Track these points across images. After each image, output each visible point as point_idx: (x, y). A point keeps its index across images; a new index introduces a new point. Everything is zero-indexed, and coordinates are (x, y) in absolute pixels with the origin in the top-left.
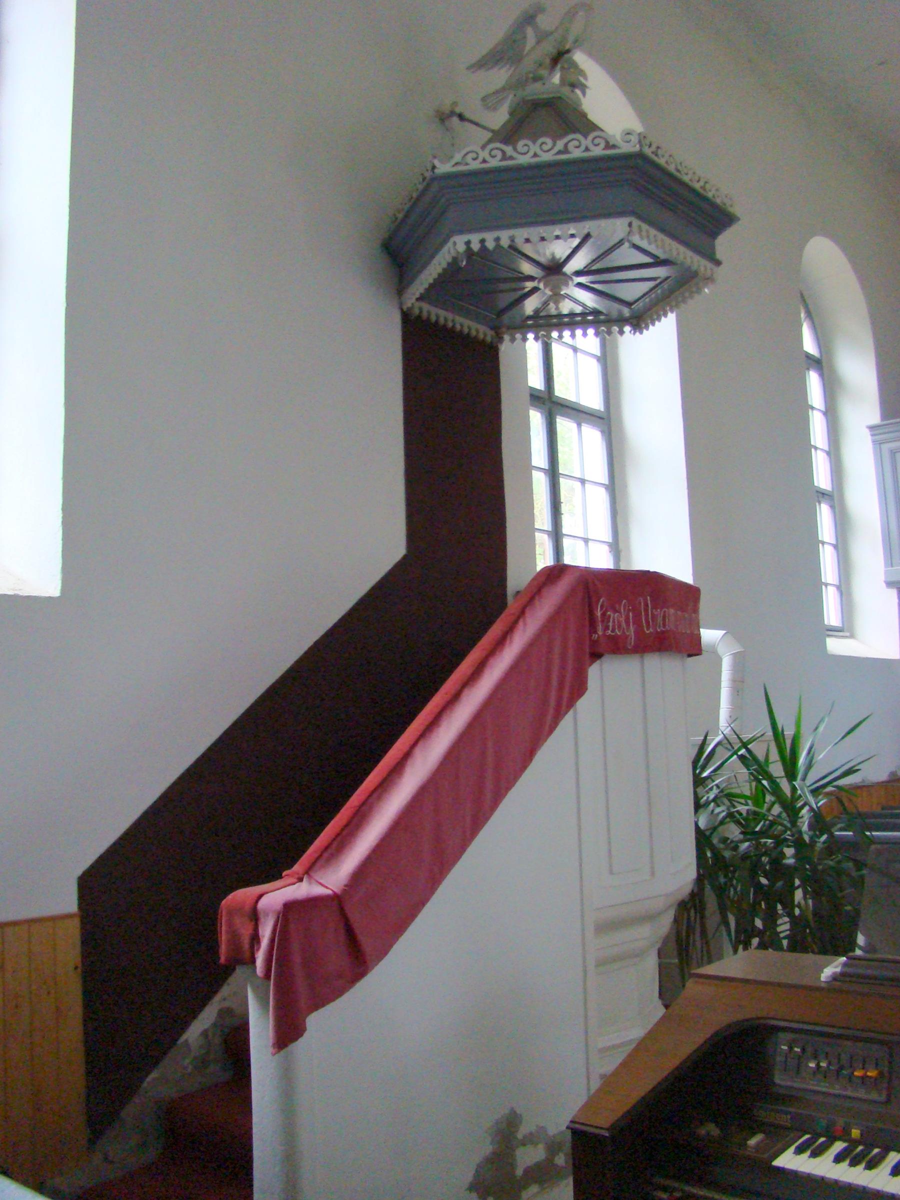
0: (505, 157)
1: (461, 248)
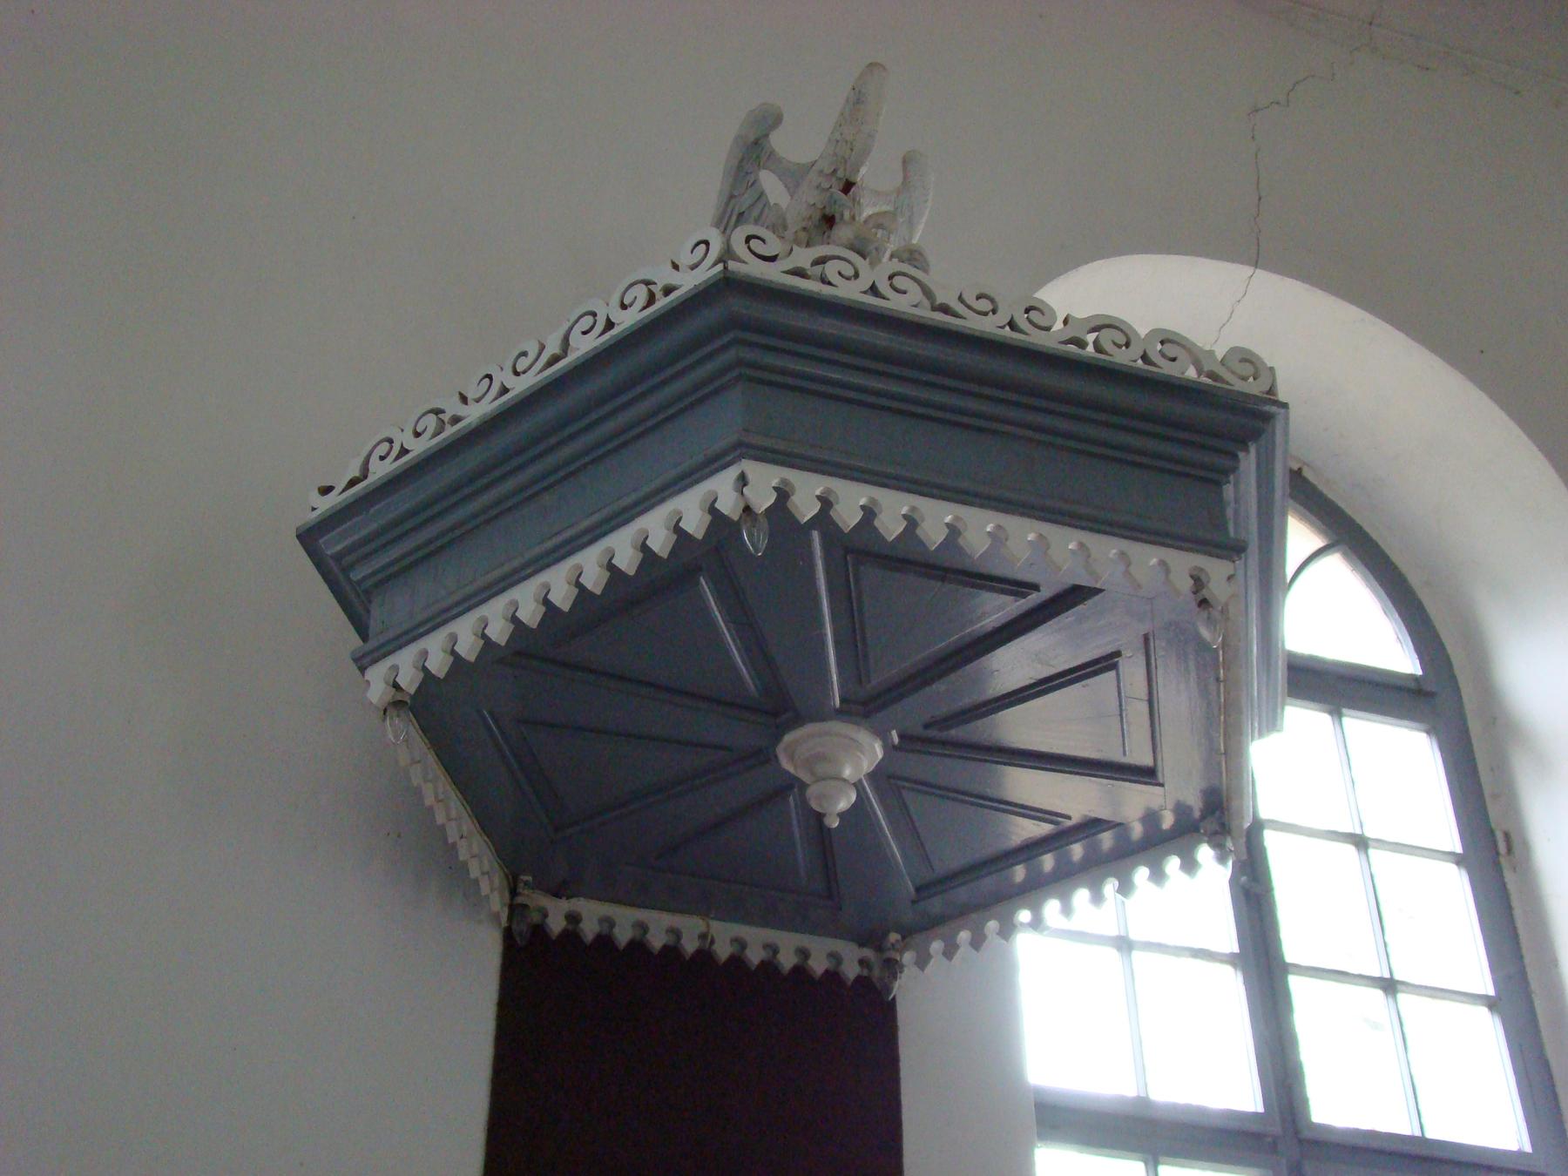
1: (763, 500)
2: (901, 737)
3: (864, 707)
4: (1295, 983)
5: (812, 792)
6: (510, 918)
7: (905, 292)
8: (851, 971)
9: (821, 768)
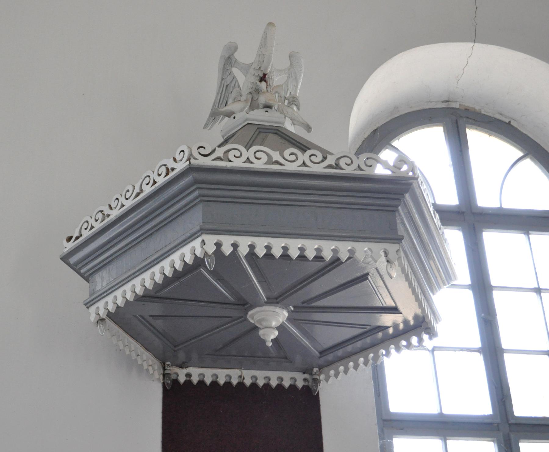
0: (270, 161)
1: (211, 249)
2: (294, 307)
3: (275, 300)
4: (507, 357)
5: (261, 332)
6: (164, 379)
7: (260, 159)
8: (300, 384)
9: (264, 324)
